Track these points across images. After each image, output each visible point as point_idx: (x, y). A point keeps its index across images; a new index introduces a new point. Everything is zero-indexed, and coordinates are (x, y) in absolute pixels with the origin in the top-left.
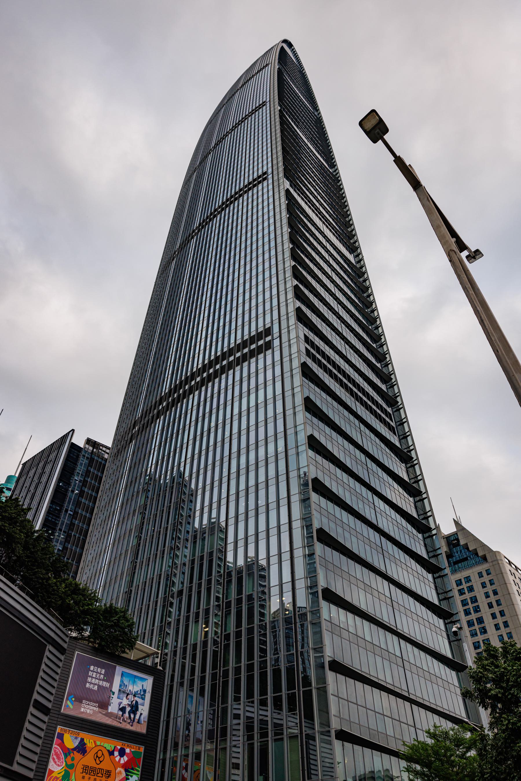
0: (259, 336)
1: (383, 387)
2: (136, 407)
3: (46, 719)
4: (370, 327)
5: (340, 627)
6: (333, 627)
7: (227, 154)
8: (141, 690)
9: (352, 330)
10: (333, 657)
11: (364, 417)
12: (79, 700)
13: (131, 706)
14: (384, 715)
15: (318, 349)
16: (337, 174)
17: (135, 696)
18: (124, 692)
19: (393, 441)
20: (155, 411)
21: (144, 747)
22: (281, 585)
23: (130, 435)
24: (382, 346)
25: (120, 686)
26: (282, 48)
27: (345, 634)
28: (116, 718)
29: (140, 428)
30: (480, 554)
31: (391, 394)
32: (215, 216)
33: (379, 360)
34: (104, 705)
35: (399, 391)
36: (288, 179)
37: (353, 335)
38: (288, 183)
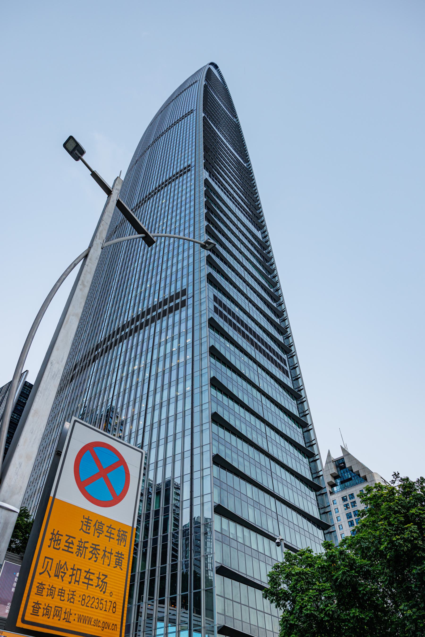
0: (177, 296)
1: (277, 321)
4: (269, 276)
5: (229, 537)
6: (223, 538)
7: (161, 150)
9: (253, 276)
10: (222, 563)
11: (262, 363)
14: (264, 612)
15: (225, 307)
16: (250, 168)
19: (286, 382)
20: (109, 343)
22: (183, 453)
23: (71, 375)
24: (277, 290)
26: (209, 69)
27: (234, 544)
30: (362, 475)
31: (282, 326)
32: (149, 199)
33: (275, 301)
35: (300, 374)
36: (207, 170)
37: (253, 280)
38: (208, 174)
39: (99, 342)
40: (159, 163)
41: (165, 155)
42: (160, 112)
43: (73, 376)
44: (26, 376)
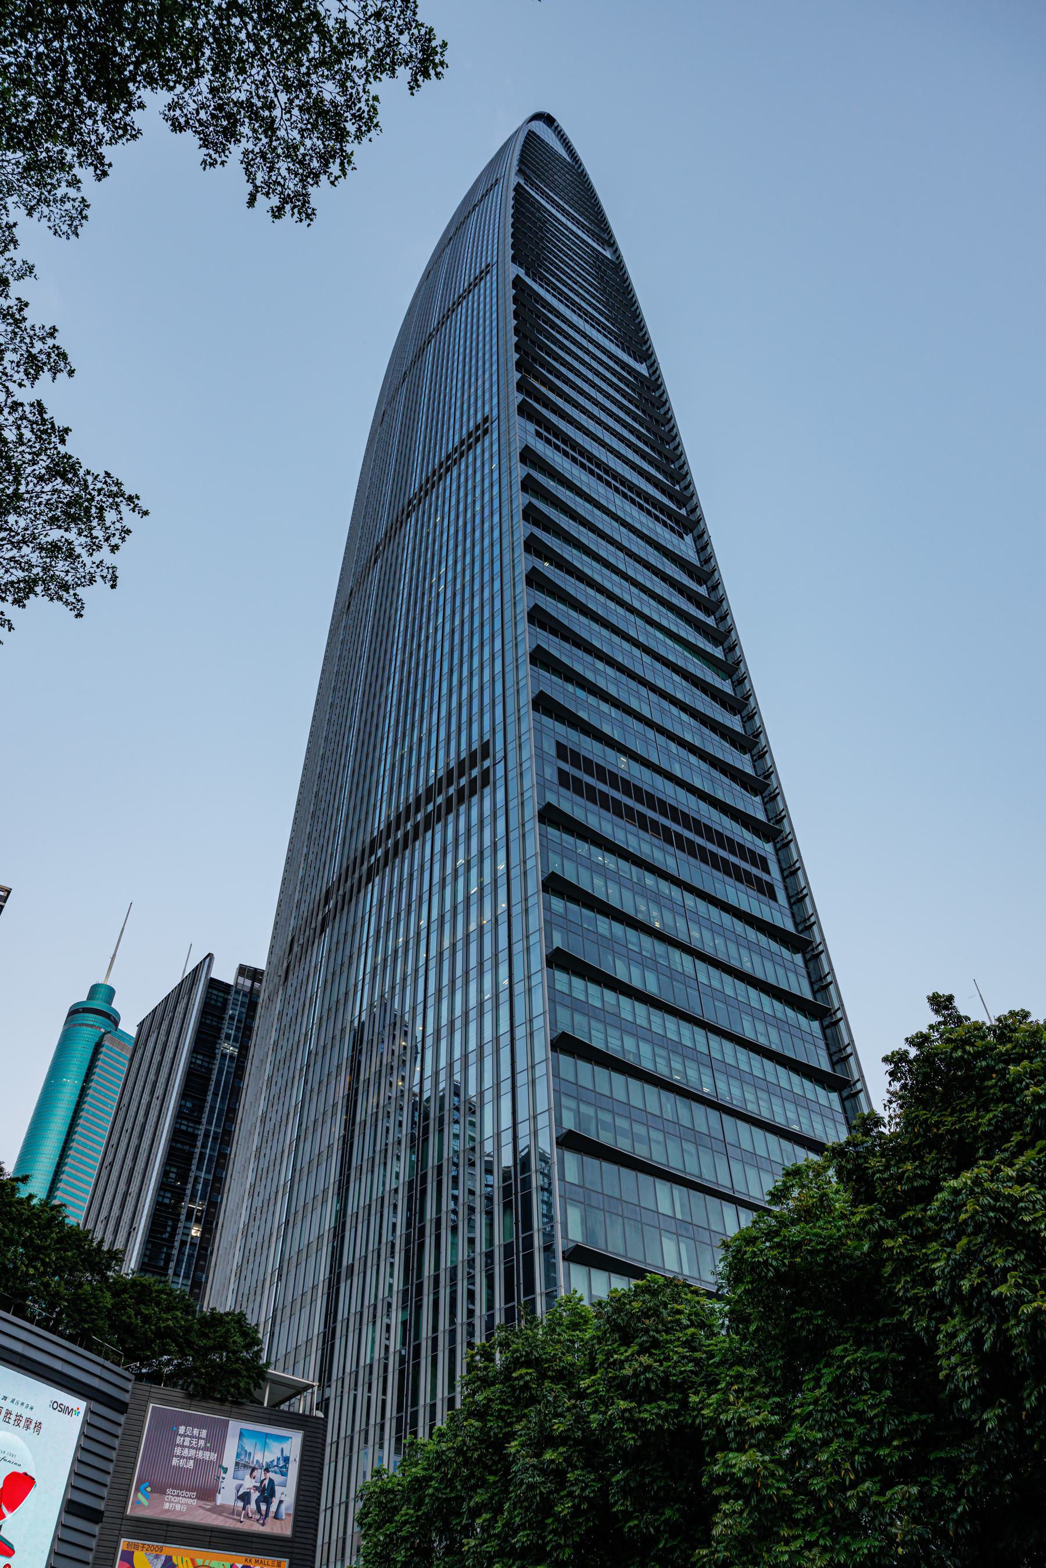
2: (321, 869)
3: (96, 1529)
8: (278, 1459)
12: (160, 1489)
13: (261, 1489)
15: (589, 766)
17: (267, 1470)
18: (245, 1466)
20: (400, 834)
21: (287, 1560)
23: (320, 917)
25: (238, 1455)
28: (233, 1513)
29: (337, 902)
31: (722, 629)
32: (448, 469)
34: (207, 1493)
39: (375, 834)
40: (460, 376)
41: (474, 352)
42: (446, 241)
43: (324, 919)
44: (209, 967)
